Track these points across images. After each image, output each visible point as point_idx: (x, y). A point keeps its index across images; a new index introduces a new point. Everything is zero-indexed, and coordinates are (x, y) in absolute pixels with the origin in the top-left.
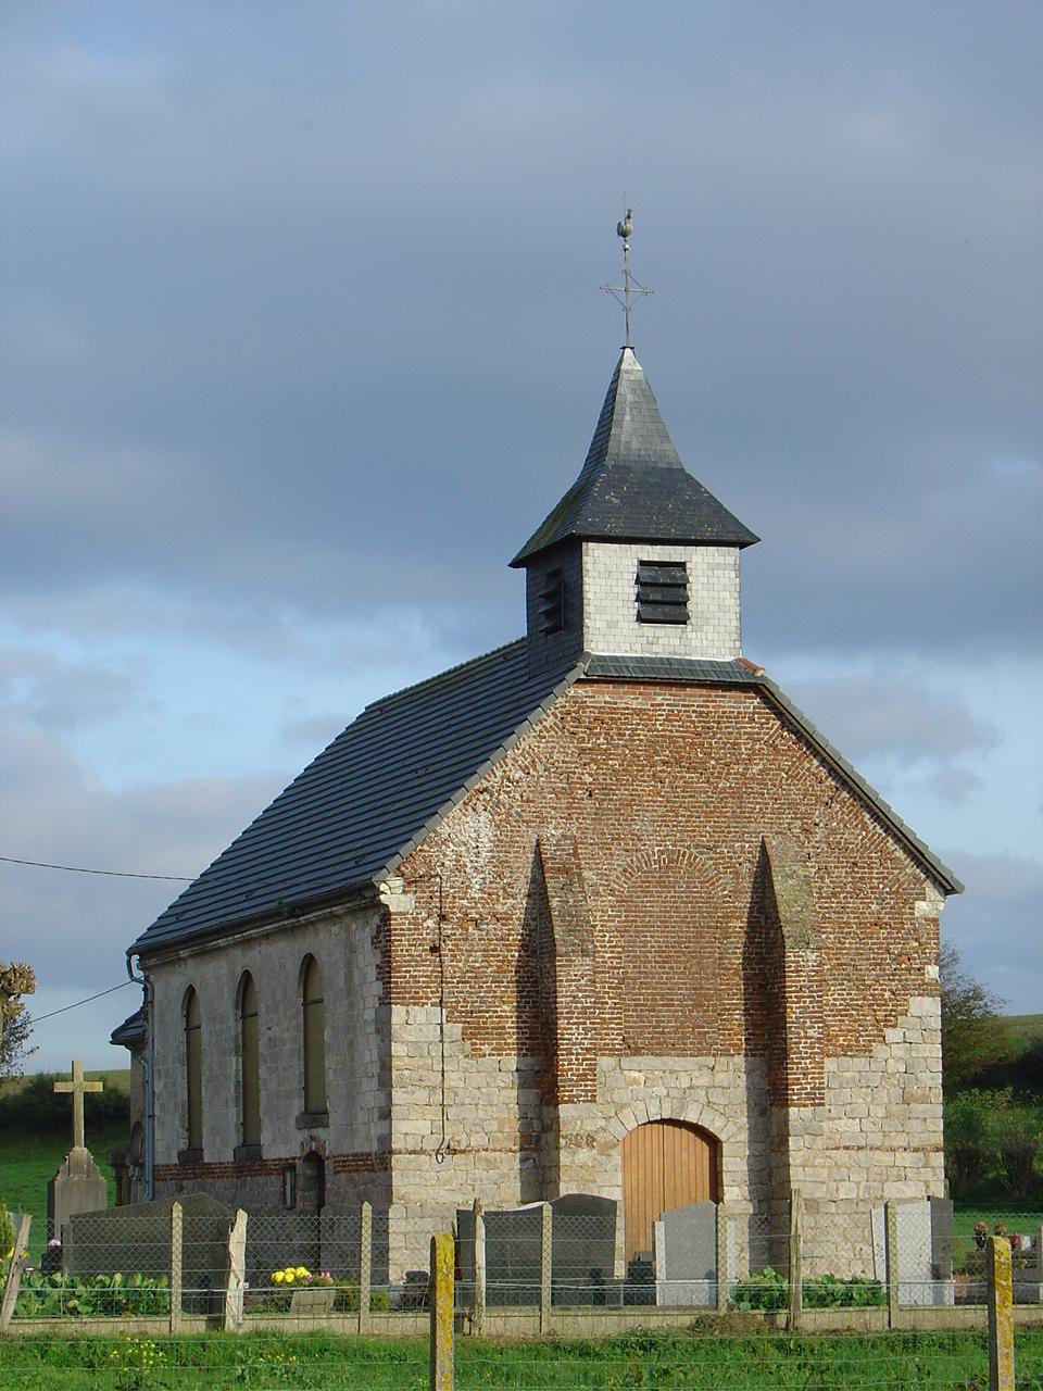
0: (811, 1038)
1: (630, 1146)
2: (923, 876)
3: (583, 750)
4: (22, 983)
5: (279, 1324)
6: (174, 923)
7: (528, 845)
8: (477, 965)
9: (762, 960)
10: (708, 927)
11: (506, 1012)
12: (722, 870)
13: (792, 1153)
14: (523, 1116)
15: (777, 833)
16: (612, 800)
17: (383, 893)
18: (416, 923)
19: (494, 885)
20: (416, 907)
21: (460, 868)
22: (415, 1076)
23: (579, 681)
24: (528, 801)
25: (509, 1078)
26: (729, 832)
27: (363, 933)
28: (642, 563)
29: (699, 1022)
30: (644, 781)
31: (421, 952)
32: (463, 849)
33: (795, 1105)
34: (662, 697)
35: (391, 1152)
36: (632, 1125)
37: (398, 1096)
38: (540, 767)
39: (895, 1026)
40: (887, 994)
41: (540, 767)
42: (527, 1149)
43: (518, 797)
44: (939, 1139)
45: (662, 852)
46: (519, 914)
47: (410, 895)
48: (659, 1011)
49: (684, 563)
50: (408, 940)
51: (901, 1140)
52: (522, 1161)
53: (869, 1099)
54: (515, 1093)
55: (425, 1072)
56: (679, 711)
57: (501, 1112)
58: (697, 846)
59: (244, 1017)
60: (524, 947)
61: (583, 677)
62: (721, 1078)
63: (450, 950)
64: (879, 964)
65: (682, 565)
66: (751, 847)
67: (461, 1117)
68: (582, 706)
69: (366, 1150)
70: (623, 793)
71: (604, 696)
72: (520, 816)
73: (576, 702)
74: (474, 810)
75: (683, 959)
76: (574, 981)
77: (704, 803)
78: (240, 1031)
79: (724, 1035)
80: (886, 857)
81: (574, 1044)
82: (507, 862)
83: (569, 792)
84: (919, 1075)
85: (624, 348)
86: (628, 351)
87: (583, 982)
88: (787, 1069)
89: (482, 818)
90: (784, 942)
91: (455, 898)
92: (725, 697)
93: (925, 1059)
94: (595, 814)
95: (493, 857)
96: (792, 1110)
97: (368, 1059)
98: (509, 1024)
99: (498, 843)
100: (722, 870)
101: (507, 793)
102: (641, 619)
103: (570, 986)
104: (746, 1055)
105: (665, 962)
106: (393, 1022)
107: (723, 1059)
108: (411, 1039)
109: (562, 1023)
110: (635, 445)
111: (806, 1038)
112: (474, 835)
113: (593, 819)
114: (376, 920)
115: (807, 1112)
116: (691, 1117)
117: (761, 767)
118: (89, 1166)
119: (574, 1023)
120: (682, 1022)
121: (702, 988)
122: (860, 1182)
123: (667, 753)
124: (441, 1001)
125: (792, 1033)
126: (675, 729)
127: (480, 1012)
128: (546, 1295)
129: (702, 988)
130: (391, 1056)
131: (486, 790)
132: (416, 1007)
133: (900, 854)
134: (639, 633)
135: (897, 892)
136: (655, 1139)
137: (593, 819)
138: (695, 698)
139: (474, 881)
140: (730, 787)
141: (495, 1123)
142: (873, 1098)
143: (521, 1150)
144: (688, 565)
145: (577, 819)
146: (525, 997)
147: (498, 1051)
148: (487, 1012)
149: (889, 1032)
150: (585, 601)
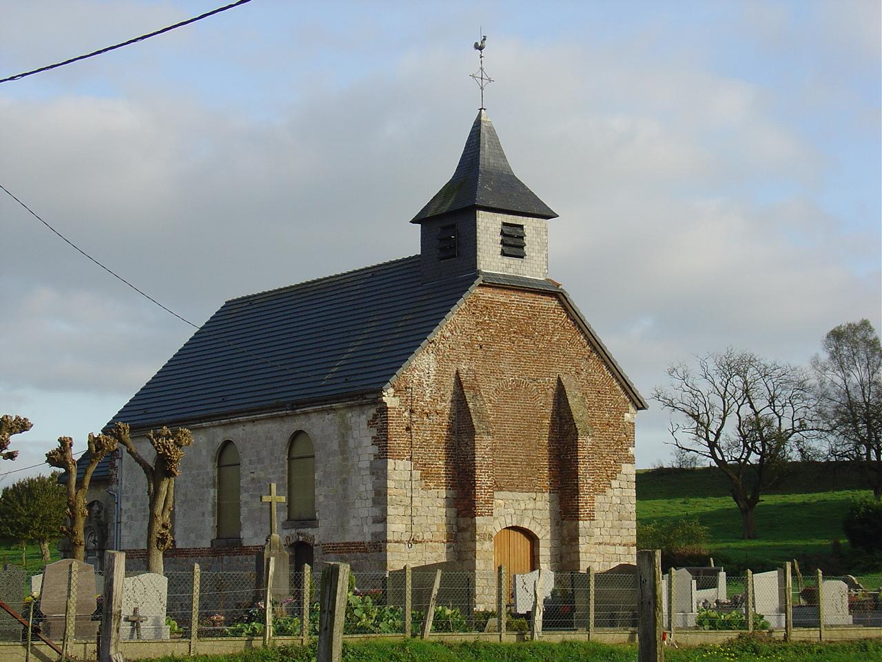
0: (589, 484)
1: (497, 540)
2: (628, 400)
3: (478, 323)
4: (186, 439)
5: (573, 637)
6: (143, 414)
7: (452, 373)
8: (428, 438)
9: (558, 441)
10: (534, 422)
11: (440, 465)
12: (540, 392)
13: (581, 546)
14: (448, 524)
15: (565, 373)
16: (491, 351)
17: (384, 396)
18: (400, 414)
19: (436, 395)
20: (400, 405)
21: (420, 384)
22: (398, 499)
23: (480, 285)
24: (453, 349)
25: (442, 502)
26: (544, 372)
27: (360, 421)
28: (504, 224)
29: (529, 474)
30: (506, 342)
31: (401, 429)
32: (422, 373)
33: (583, 520)
34: (515, 297)
35: (386, 542)
36: (499, 529)
37: (390, 510)
38: (458, 331)
39: (615, 479)
40: (612, 462)
41: (458, 331)
42: (451, 541)
43: (448, 346)
44: (634, 540)
45: (513, 381)
46: (447, 411)
47: (397, 398)
48: (511, 467)
49: (523, 226)
50: (396, 423)
51: (618, 540)
52: (448, 548)
53: (604, 518)
54: (444, 510)
55: (403, 498)
56: (522, 305)
57: (438, 520)
58: (529, 378)
59: (219, 467)
60: (449, 429)
61: (482, 283)
62: (539, 504)
63: (416, 430)
64: (609, 446)
65: (521, 227)
66: (554, 380)
67: (420, 522)
68: (478, 299)
69: (359, 539)
70: (496, 348)
71: (488, 294)
72: (449, 357)
73: (475, 296)
74: (427, 352)
75: (522, 439)
76: (483, 449)
77: (533, 355)
78: (216, 473)
79: (540, 481)
80: (613, 389)
81: (483, 484)
82: (442, 382)
83: (471, 345)
84: (626, 505)
85: (481, 109)
86: (483, 110)
87: (487, 450)
88: (578, 500)
89: (431, 357)
90: (577, 432)
91: (418, 400)
92: (542, 298)
93: (628, 497)
94: (483, 358)
95: (436, 379)
96: (581, 522)
97: (362, 488)
98: (442, 472)
99: (438, 371)
100: (540, 392)
101: (443, 344)
102: (503, 254)
103: (481, 451)
104: (550, 492)
105: (513, 440)
106: (388, 468)
107: (540, 494)
108: (397, 478)
109: (478, 471)
110: (492, 161)
111: (587, 483)
112: (427, 366)
113: (483, 361)
114: (373, 411)
115: (587, 523)
116: (526, 526)
117: (558, 337)
118: (280, 545)
119: (483, 472)
120: (522, 474)
121: (530, 455)
122: (600, 562)
123: (516, 327)
124: (411, 458)
125: (581, 481)
126: (520, 315)
127: (429, 464)
128: (592, 623)
129: (530, 455)
130: (387, 487)
131: (433, 341)
132: (399, 461)
133: (618, 388)
134: (501, 261)
135: (617, 408)
136: (506, 536)
137: (483, 361)
138: (529, 298)
139: (427, 391)
140: (544, 347)
141: (436, 527)
142: (606, 517)
143: (447, 542)
144: (524, 227)
145: (475, 360)
146: (450, 457)
147: (437, 486)
148: (432, 464)
149: (613, 482)
150: (478, 242)
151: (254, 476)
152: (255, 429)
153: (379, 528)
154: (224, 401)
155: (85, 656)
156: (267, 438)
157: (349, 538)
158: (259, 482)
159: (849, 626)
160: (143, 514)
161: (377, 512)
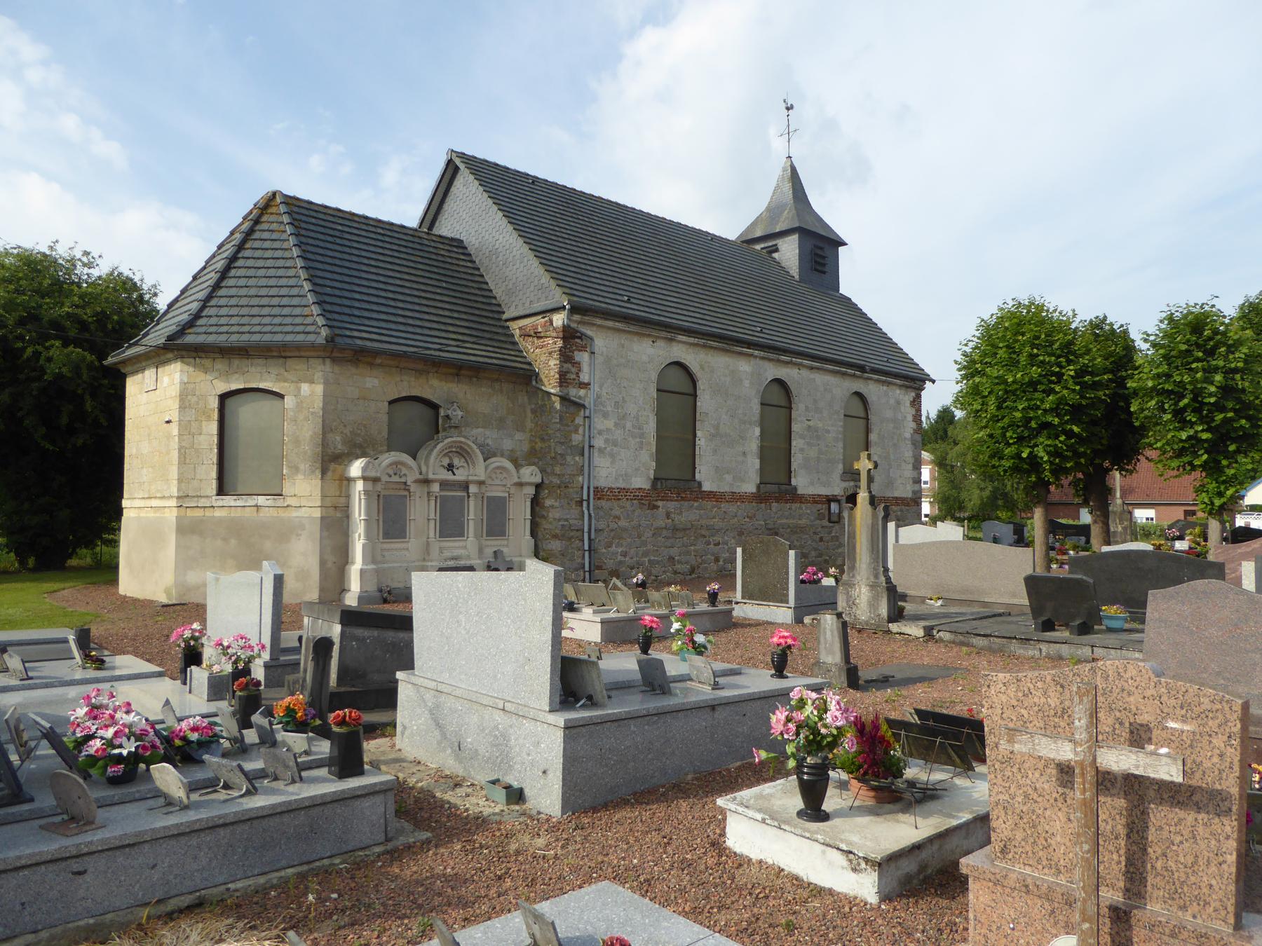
151: (811, 423)
152: (812, 376)
153: (916, 487)
154: (887, 362)
155: (265, 699)
156: (825, 390)
157: (897, 494)
158: (817, 431)
159: (545, 711)
160: (638, 440)
161: (915, 474)
